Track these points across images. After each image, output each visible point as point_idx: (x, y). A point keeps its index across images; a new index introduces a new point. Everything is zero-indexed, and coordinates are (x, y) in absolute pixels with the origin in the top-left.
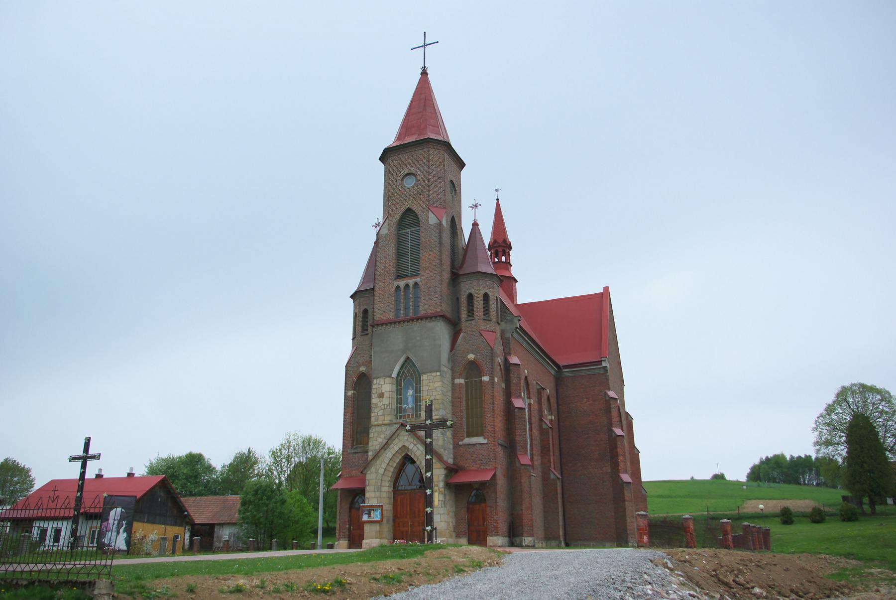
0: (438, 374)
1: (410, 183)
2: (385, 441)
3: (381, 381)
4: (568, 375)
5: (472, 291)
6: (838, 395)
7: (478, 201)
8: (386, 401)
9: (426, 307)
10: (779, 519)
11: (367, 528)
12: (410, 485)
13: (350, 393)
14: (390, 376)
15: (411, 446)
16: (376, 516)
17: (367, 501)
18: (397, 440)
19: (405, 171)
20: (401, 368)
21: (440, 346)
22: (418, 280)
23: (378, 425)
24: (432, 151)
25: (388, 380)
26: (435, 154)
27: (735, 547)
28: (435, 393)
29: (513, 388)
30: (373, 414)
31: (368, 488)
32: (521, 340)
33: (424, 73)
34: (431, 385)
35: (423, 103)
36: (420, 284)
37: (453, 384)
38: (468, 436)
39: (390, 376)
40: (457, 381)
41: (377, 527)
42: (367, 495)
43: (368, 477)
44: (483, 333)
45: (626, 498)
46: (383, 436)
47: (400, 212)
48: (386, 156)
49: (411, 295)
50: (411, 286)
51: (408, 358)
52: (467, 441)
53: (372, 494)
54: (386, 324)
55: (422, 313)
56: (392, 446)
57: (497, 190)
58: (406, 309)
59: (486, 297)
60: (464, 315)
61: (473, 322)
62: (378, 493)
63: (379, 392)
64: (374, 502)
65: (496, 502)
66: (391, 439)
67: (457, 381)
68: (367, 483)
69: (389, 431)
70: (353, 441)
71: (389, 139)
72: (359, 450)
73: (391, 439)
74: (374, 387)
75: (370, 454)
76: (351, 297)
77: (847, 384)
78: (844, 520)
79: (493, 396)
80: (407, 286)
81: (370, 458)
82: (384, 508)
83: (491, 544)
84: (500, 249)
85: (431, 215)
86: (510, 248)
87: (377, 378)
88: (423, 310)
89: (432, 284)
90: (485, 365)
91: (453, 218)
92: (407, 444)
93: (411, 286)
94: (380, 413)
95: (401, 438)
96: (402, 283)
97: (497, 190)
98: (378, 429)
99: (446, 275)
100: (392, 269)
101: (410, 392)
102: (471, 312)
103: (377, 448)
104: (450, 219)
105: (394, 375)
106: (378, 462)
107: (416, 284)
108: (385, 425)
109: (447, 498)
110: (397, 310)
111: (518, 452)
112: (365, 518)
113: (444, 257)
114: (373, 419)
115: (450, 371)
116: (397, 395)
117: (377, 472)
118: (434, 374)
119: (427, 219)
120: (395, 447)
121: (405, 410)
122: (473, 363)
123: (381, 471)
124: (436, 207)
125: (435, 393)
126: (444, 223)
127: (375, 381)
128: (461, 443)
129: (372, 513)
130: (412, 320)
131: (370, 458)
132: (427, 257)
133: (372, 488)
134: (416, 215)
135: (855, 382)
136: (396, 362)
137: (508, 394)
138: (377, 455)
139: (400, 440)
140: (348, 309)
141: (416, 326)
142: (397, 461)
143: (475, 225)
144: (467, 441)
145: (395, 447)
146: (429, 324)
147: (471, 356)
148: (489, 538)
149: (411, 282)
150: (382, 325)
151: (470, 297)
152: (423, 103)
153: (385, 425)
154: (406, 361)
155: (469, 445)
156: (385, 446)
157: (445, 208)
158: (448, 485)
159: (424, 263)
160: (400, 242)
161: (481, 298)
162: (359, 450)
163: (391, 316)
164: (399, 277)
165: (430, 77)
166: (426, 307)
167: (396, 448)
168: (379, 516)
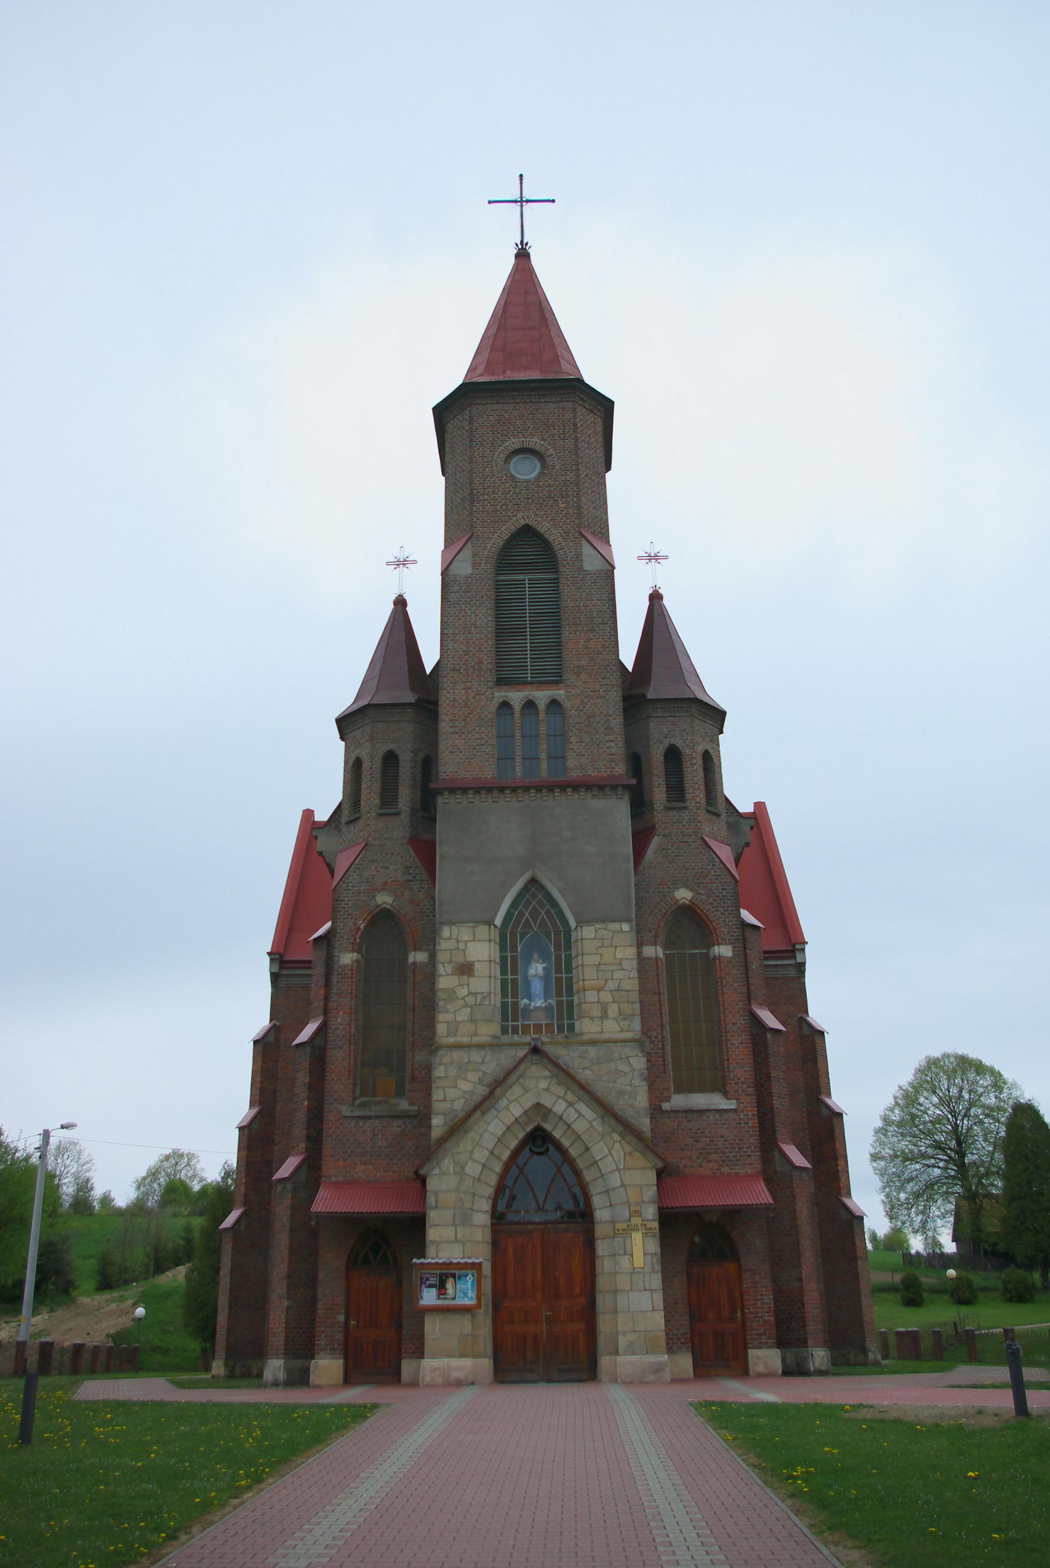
1: (526, 470)
2: (482, 1090)
3: (465, 933)
5: (679, 743)
6: (921, 1071)
10: (898, 1297)
11: (433, 1327)
12: (540, 1209)
14: (490, 923)
15: (560, 1107)
16: (464, 1292)
17: (431, 1250)
18: (517, 1090)
19: (515, 443)
22: (560, 694)
23: (459, 1046)
24: (581, 412)
25: (483, 931)
27: (901, 1357)
30: (441, 1017)
31: (432, 1216)
33: (523, 255)
35: (523, 312)
36: (567, 704)
38: (678, 1090)
39: (490, 923)
40: (649, 951)
41: (464, 1325)
42: (431, 1234)
43: (432, 1184)
46: (473, 1076)
47: (506, 531)
51: (533, 881)
52: (679, 1101)
53: (449, 1233)
56: (503, 1102)
58: (531, 759)
61: (685, 815)
62: (457, 1232)
63: (459, 959)
64: (455, 1255)
66: (497, 1086)
67: (649, 951)
68: (431, 1199)
69: (492, 1064)
72: (375, 1110)
73: (497, 1086)
75: (436, 1121)
77: (937, 1053)
78: (1010, 1300)
80: (530, 705)
81: (436, 1132)
83: (761, 1369)
87: (452, 923)
88: (575, 767)
92: (547, 1101)
93: (517, 707)
94: (463, 1015)
96: (516, 697)
98: (456, 1055)
100: (488, 659)
101: (537, 968)
103: (458, 1105)
105: (498, 921)
107: (554, 703)
108: (479, 1046)
110: (505, 759)
111: (779, 1137)
112: (429, 1297)
114: (441, 1029)
116: (504, 971)
117: (461, 1173)
118: (614, 926)
119: (578, 557)
120: (513, 1107)
121: (527, 1009)
122: (690, 913)
123: (473, 1170)
125: (618, 975)
127: (446, 932)
128: (666, 1106)
129: (449, 1285)
131: (436, 1132)
133: (448, 1215)
135: (950, 1050)
136: (505, 888)
138: (458, 1127)
139: (526, 1090)
141: (560, 804)
143: (655, 598)
144: (679, 1101)
145: (513, 1107)
147: (683, 895)
148: (752, 1353)
149: (542, 696)
150: (464, 791)
151: (673, 755)
152: (523, 312)
153: (479, 1046)
154: (525, 889)
155: (688, 1111)
160: (503, 603)
162: (375, 1110)
163: (489, 772)
164: (501, 682)
165: (537, 262)
167: (517, 1111)
168: (472, 1294)
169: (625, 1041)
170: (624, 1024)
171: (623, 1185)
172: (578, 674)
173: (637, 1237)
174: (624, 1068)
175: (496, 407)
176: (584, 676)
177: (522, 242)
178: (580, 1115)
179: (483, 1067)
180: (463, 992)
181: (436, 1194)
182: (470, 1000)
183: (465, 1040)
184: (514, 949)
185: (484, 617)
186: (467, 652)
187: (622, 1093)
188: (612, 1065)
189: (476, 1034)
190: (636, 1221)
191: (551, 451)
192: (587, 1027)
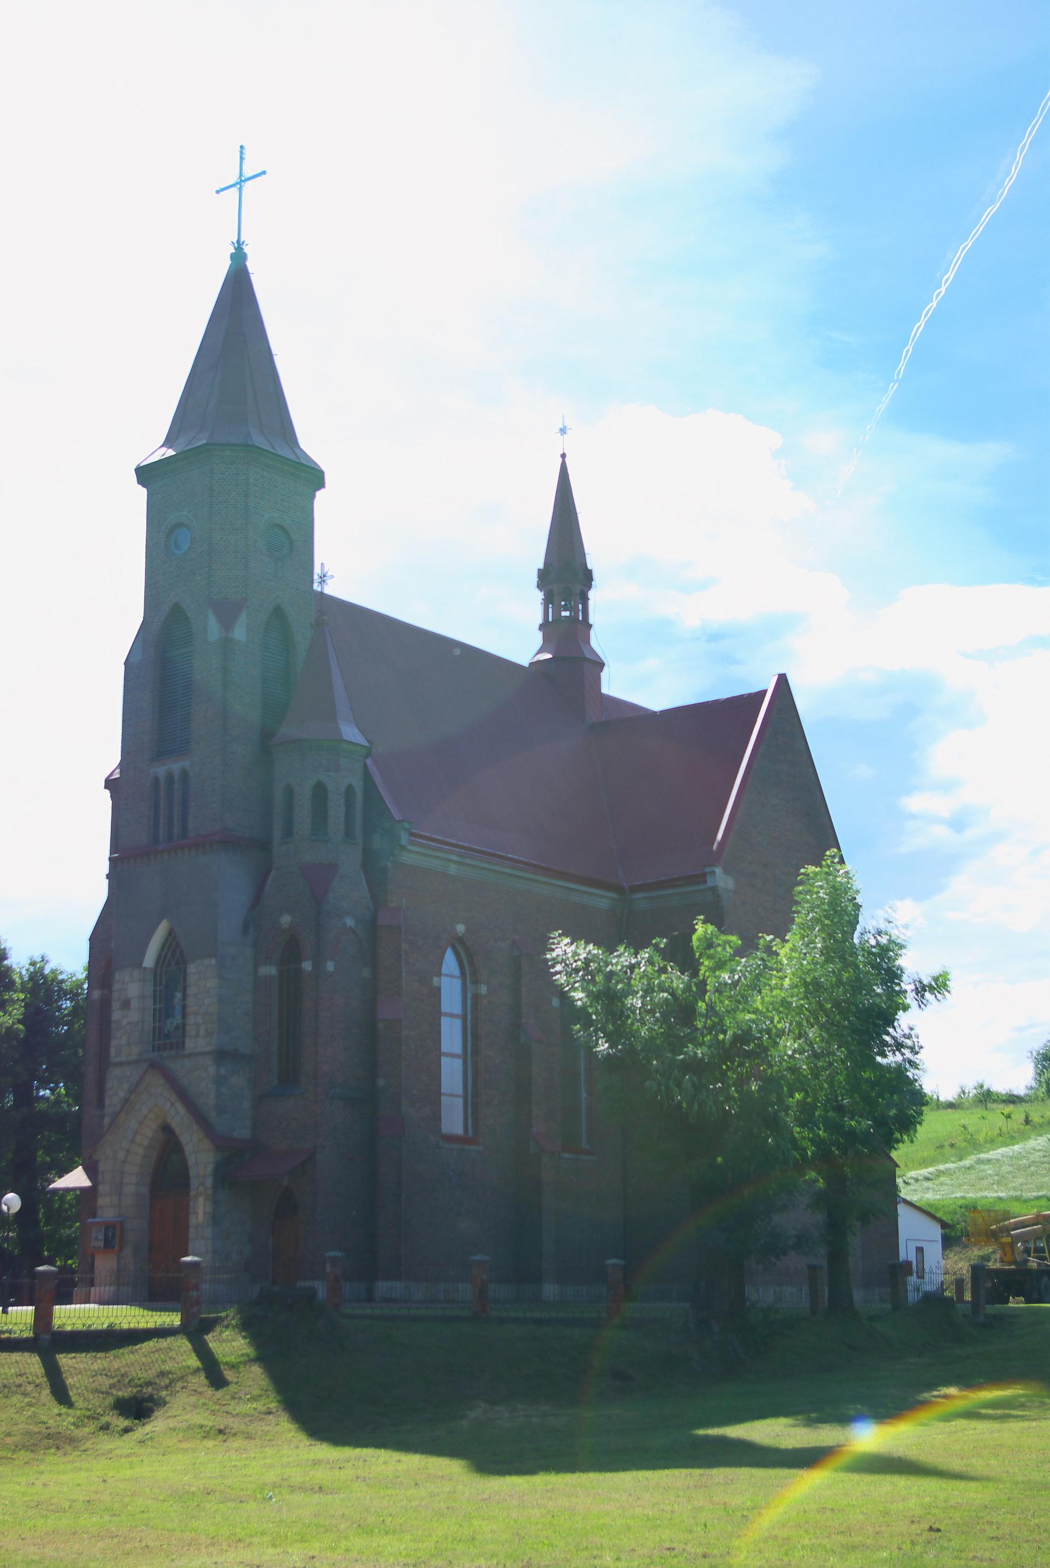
0: (213, 961)
8: (134, 1016)
23: (120, 1064)
57: (563, 431)
59: (320, 792)
60: (277, 834)
74: (116, 986)
94: (124, 1042)
97: (563, 431)
108: (129, 1063)
116: (155, 1003)
151: (290, 792)
173: (201, 1200)
177: (238, 241)
178: (177, 1112)
180: (124, 1022)
184: (161, 985)
190: (201, 1189)
192: (189, 1044)
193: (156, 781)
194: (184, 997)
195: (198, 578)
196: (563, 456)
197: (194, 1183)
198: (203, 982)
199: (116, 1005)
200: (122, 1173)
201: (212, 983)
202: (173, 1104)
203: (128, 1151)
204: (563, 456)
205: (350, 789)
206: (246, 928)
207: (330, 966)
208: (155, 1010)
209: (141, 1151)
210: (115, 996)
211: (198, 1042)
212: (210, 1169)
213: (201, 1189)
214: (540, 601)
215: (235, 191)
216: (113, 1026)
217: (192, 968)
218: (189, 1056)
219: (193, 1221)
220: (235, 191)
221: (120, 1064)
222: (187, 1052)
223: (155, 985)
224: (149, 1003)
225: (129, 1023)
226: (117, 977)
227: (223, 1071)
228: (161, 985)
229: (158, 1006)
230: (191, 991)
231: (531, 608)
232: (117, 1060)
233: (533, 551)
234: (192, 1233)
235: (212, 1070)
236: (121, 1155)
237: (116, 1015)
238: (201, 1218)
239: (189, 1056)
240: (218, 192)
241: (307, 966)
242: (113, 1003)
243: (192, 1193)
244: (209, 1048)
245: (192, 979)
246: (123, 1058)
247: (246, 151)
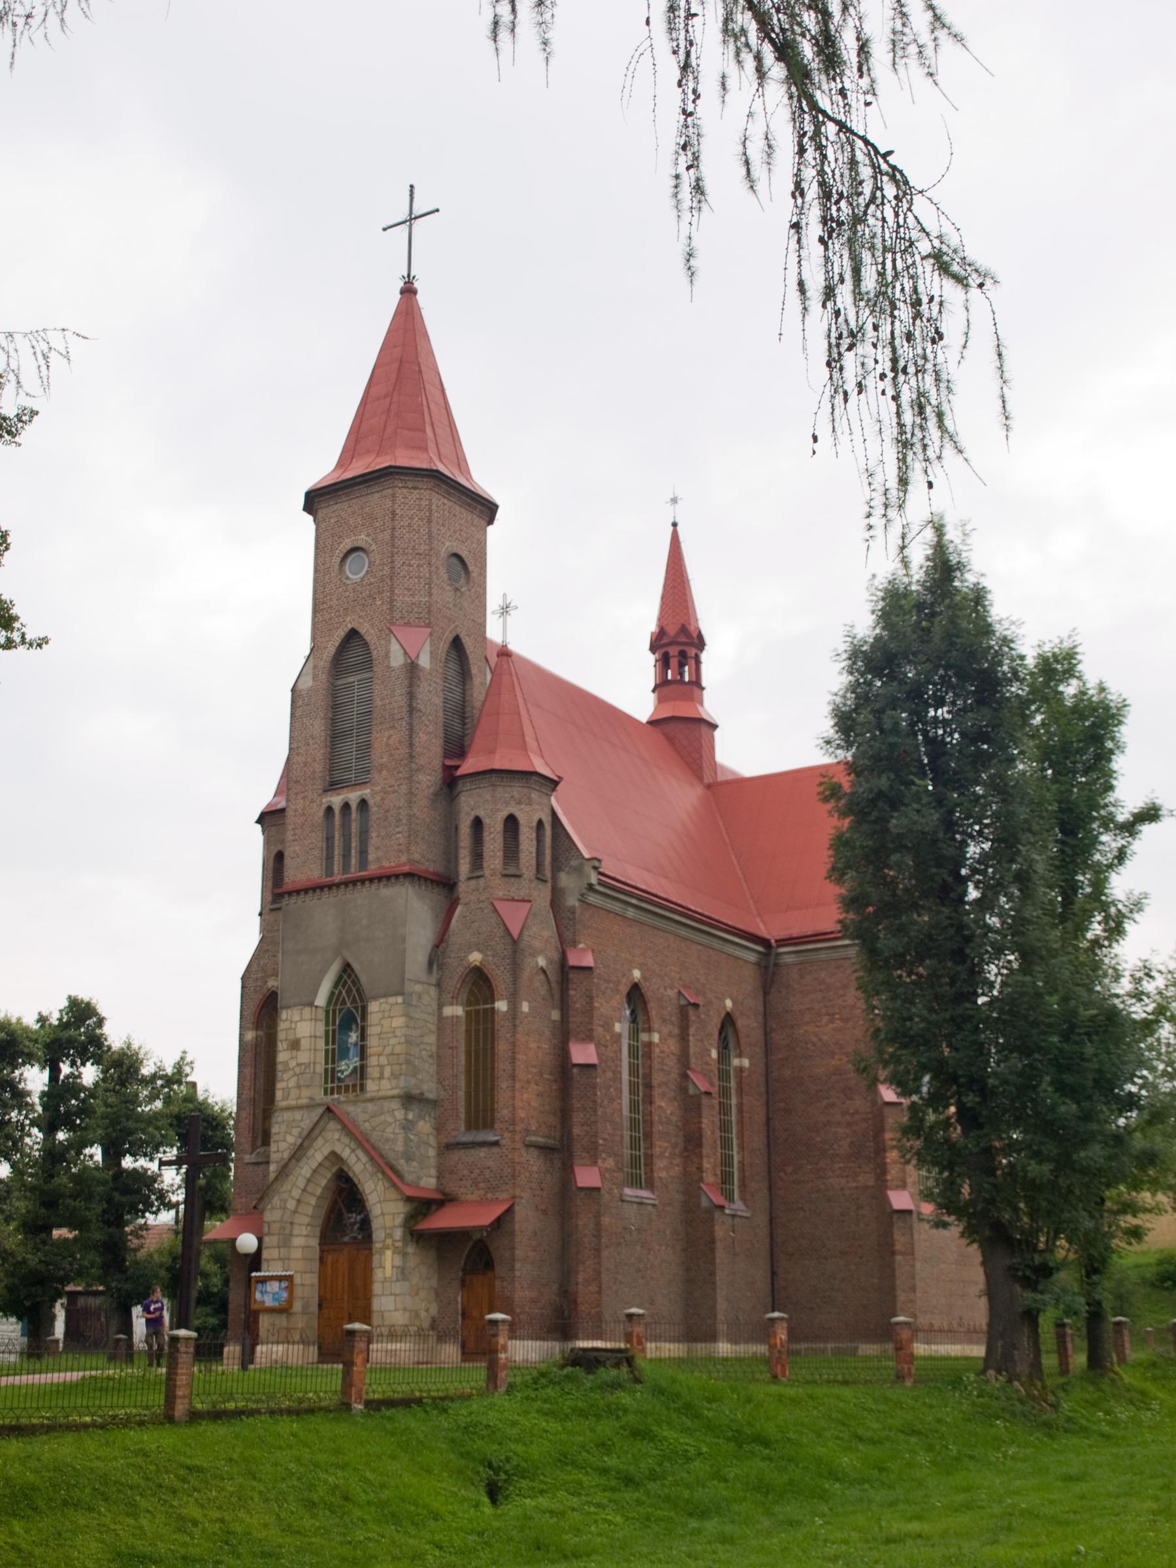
0: (400, 999)
2: (299, 1141)
4: (789, 959)
5: (481, 813)
7: (679, 495)
8: (304, 1057)
9: (380, 853)
13: (250, 1035)
15: (346, 1154)
17: (264, 1265)
18: (320, 1141)
19: (347, 544)
20: (336, 985)
21: (403, 940)
22: (366, 792)
23: (288, 1108)
24: (401, 493)
26: (409, 499)
28: (393, 1041)
29: (575, 1020)
30: (279, 1085)
32: (617, 907)
33: (409, 291)
34: (386, 1022)
37: (441, 1018)
40: (448, 1011)
44: (510, 907)
45: (898, 1247)
46: (296, 1131)
47: (341, 633)
48: (314, 501)
49: (355, 827)
50: (354, 806)
54: (306, 891)
55: (373, 868)
56: (311, 1152)
57: (674, 501)
59: (511, 822)
60: (464, 868)
61: (482, 881)
63: (291, 1037)
65: (512, 1269)
66: (309, 1137)
67: (448, 1011)
69: (307, 1120)
70: (254, 1139)
71: (321, 464)
73: (309, 1137)
74: (282, 1026)
76: (258, 821)
79: (514, 1044)
80: (346, 806)
81: (272, 1176)
82: (297, 1280)
84: (674, 651)
85: (395, 647)
86: (700, 643)
87: (288, 1007)
89: (397, 795)
90: (500, 978)
91: (457, 644)
93: (354, 806)
94: (292, 1083)
95: (328, 1135)
96: (336, 800)
97: (674, 501)
98: (287, 1115)
99: (428, 780)
100: (319, 767)
102: (477, 857)
103: (286, 1155)
104: (444, 646)
105: (321, 1000)
106: (287, 1186)
107: (363, 803)
108: (300, 1108)
109: (412, 1261)
113: (421, 738)
115: (433, 991)
116: (327, 1044)
118: (392, 1000)
119: (387, 655)
120: (318, 1154)
124: (408, 624)
125: (393, 1041)
126: (424, 661)
130: (354, 882)
132: (386, 740)
134: (366, 644)
137: (564, 1035)
138: (284, 1170)
140: (252, 846)
141: (361, 897)
142: (324, 1182)
145: (318, 1154)
146: (386, 892)
147: (475, 957)
149: (353, 796)
151: (478, 823)
153: (300, 1108)
156: (299, 1152)
157: (428, 625)
158: (416, 1235)
159: (379, 755)
161: (499, 827)
164: (333, 786)
166: (380, 853)
167: (319, 1157)
169: (393, 1097)
170: (394, 1082)
171: (383, 1214)
172: (380, 771)
173: (389, 1253)
174: (390, 1119)
175: (335, 507)
176: (384, 772)
177: (409, 276)
178: (359, 1159)
179: (302, 1124)
180: (293, 1064)
181: (269, 1224)
182: (298, 1070)
183: (293, 1103)
184: (334, 1024)
185: (318, 727)
186: (305, 764)
187: (388, 1140)
188: (383, 1117)
189: (300, 1098)
190: (389, 1241)
191: (374, 547)
192: (371, 1086)
193: (329, 809)
194: (363, 1036)
195: (379, 603)
196: (675, 525)
197: (378, 1235)
198: (386, 1020)
199: (281, 1046)
200: (292, 1223)
201: (399, 1022)
202: (353, 1151)
203: (299, 1201)
204: (675, 525)
205: (540, 823)
206: (430, 964)
207: (525, 1007)
208: (327, 1051)
209: (313, 1201)
210: (281, 1036)
211: (382, 1083)
212: (399, 1220)
213: (389, 1241)
214: (653, 663)
215: (416, 212)
216: (280, 1067)
217: (373, 1007)
218: (372, 1100)
219: (378, 1275)
220: (416, 212)
221: (288, 1108)
222: (368, 1095)
223: (327, 1025)
224: (321, 1044)
225: (299, 1065)
226: (284, 1015)
227: (410, 1116)
228: (334, 1024)
229: (330, 1047)
230: (372, 1031)
231: (646, 667)
232: (285, 1103)
233: (645, 616)
234: (377, 1288)
235: (400, 1114)
236: (291, 1205)
237: (282, 1056)
238: (389, 1272)
239: (372, 1100)
240: (385, 229)
241: (502, 1006)
242: (279, 1044)
243: (377, 1246)
244: (396, 1092)
245: (373, 1018)
246: (292, 1102)
247: (416, 191)
